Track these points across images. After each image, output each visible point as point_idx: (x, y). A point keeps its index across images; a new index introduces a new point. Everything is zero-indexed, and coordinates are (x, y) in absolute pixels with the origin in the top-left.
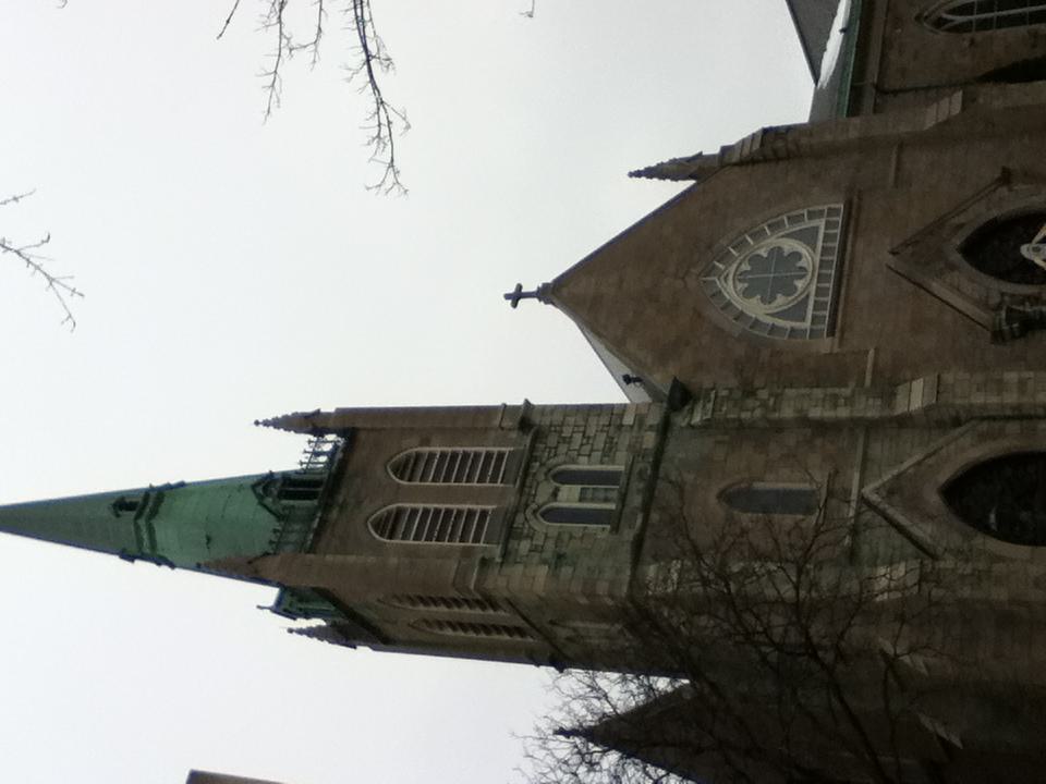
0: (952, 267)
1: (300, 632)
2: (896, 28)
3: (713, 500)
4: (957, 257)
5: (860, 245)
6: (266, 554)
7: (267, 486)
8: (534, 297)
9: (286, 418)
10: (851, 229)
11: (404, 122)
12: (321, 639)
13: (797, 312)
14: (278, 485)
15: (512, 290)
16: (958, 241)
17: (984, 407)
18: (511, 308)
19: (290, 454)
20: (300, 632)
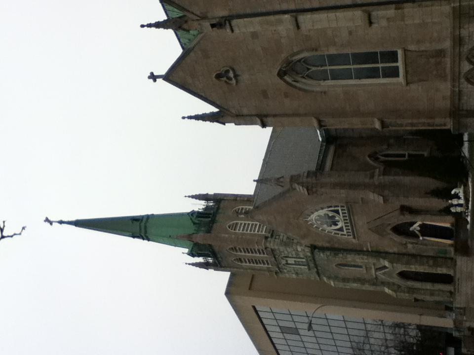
0: (389, 234)
1: (193, 264)
2: (285, 71)
3: (334, 267)
4: (391, 232)
5: (356, 218)
6: (194, 233)
7: (193, 213)
8: (193, 119)
9: (196, 195)
10: (351, 214)
11: (159, 81)
12: (196, 266)
13: (337, 212)
14: (196, 214)
15: (151, 80)
16: (390, 227)
17: (451, 64)
18: (182, 116)
19: (199, 206)
20: (193, 264)
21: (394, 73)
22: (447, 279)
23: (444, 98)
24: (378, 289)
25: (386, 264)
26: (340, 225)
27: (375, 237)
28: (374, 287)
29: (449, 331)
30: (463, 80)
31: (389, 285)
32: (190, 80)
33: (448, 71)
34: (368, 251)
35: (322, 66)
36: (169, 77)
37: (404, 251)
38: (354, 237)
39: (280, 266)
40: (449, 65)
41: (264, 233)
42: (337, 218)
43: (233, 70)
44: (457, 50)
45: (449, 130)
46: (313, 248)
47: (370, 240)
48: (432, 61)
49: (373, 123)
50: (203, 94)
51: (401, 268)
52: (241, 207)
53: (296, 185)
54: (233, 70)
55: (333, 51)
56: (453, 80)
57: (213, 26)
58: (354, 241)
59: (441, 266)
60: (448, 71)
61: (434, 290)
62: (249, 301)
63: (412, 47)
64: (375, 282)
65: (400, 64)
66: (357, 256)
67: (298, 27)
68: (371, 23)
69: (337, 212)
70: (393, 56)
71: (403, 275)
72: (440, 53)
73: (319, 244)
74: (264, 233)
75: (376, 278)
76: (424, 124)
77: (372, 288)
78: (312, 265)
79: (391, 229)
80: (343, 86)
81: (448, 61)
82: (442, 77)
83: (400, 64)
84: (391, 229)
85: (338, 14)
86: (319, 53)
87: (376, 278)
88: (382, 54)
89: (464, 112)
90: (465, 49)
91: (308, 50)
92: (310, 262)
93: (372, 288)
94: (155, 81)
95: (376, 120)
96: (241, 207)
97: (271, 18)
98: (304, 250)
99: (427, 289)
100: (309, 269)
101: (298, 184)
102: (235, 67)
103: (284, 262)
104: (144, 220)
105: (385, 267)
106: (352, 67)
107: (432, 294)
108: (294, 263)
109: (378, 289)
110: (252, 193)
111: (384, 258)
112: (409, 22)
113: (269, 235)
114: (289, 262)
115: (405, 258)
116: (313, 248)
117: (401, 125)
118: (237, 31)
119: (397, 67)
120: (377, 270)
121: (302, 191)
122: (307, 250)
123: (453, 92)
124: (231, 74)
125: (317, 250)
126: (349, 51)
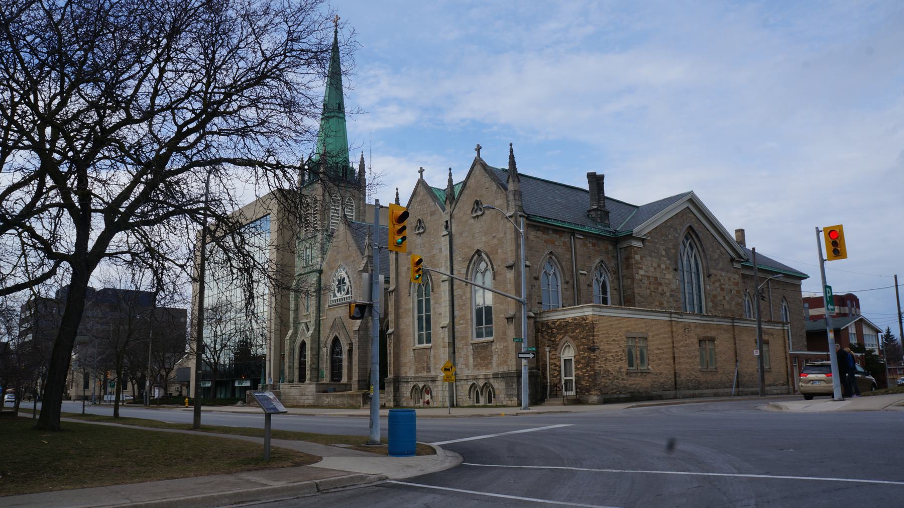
5: (344, 308)
13: (348, 293)
16: (337, 335)
21: (420, 342)
22: (302, 379)
23: (406, 372)
24: (292, 325)
25: (311, 332)
26: (338, 295)
27: (330, 323)
28: (292, 322)
29: (262, 381)
30: (414, 383)
31: (295, 333)
32: (419, 199)
33: (420, 374)
34: (320, 317)
35: (425, 294)
36: (421, 183)
37: (322, 345)
38: (329, 306)
39: (304, 242)
40: (422, 375)
41: (331, 227)
42: (343, 293)
43: (423, 233)
44: (429, 380)
45: (387, 376)
46: (320, 272)
47: (328, 318)
48: (425, 365)
49: (392, 328)
50: (410, 208)
51: (709, 360)
52: (354, 205)
53: (366, 261)
54: (423, 233)
55: (432, 302)
56: (415, 378)
57: (447, 222)
58: (327, 306)
59: (311, 373)
60: (420, 374)
61: (293, 369)
62: (274, 207)
63: (432, 351)
64: (297, 323)
65: (425, 345)
66: (315, 308)
67: (443, 281)
68: (442, 328)
69: (348, 293)
70: (428, 341)
71: (303, 344)
72: (429, 370)
73: (323, 277)
74: (331, 227)
75: (300, 323)
76: (390, 360)
77: (291, 320)
78: (307, 270)
79: (336, 336)
80: (413, 308)
81: (425, 374)
82: (417, 371)
83: (425, 345)
84: (336, 336)
85: (448, 307)
86: (431, 293)
87: (300, 323)
88: (430, 334)
89: (397, 385)
90: (430, 384)
91: (432, 286)
92: (308, 268)
93: (291, 320)
94: (419, 172)
95: (393, 330)
96: (354, 205)
97: (449, 263)
98: (317, 264)
99: (293, 363)
100: (303, 267)
101: (367, 263)
102: (425, 234)
103: (308, 245)
104: (341, 115)
105: (308, 330)
106: (424, 314)
107: (290, 367)
108: (308, 254)
109: (292, 325)
110: (120, 416)
111: (315, 330)
112: (442, 350)
113: (329, 233)
114: (308, 250)
115: (315, 346)
116: (320, 272)
117: (390, 346)
118: (443, 239)
119: (423, 343)
120: (306, 324)
121: (361, 266)
122: (318, 267)
123: (408, 378)
124: (421, 231)
125: (318, 275)
126: (432, 313)
